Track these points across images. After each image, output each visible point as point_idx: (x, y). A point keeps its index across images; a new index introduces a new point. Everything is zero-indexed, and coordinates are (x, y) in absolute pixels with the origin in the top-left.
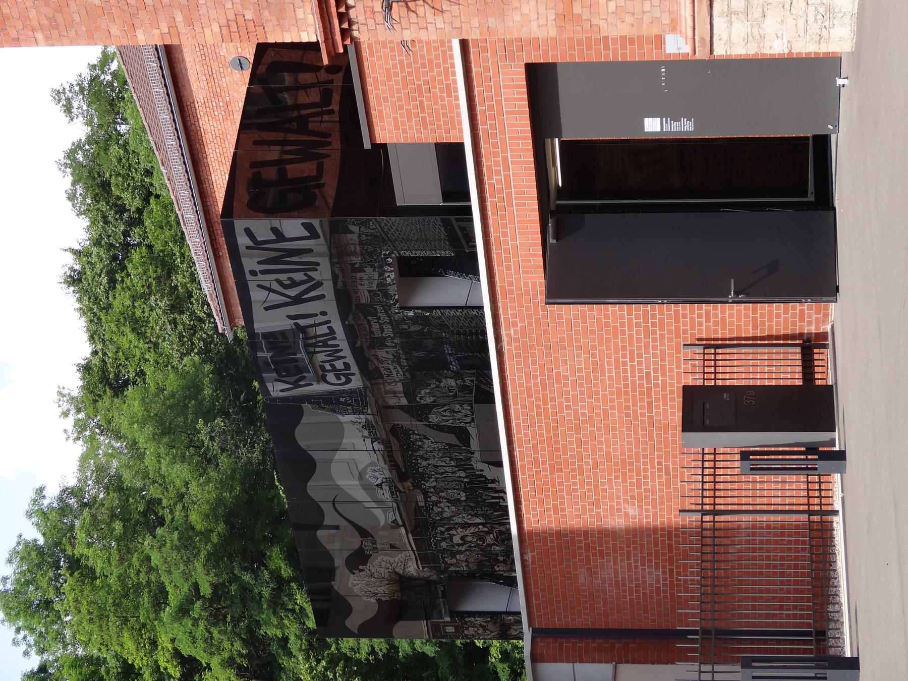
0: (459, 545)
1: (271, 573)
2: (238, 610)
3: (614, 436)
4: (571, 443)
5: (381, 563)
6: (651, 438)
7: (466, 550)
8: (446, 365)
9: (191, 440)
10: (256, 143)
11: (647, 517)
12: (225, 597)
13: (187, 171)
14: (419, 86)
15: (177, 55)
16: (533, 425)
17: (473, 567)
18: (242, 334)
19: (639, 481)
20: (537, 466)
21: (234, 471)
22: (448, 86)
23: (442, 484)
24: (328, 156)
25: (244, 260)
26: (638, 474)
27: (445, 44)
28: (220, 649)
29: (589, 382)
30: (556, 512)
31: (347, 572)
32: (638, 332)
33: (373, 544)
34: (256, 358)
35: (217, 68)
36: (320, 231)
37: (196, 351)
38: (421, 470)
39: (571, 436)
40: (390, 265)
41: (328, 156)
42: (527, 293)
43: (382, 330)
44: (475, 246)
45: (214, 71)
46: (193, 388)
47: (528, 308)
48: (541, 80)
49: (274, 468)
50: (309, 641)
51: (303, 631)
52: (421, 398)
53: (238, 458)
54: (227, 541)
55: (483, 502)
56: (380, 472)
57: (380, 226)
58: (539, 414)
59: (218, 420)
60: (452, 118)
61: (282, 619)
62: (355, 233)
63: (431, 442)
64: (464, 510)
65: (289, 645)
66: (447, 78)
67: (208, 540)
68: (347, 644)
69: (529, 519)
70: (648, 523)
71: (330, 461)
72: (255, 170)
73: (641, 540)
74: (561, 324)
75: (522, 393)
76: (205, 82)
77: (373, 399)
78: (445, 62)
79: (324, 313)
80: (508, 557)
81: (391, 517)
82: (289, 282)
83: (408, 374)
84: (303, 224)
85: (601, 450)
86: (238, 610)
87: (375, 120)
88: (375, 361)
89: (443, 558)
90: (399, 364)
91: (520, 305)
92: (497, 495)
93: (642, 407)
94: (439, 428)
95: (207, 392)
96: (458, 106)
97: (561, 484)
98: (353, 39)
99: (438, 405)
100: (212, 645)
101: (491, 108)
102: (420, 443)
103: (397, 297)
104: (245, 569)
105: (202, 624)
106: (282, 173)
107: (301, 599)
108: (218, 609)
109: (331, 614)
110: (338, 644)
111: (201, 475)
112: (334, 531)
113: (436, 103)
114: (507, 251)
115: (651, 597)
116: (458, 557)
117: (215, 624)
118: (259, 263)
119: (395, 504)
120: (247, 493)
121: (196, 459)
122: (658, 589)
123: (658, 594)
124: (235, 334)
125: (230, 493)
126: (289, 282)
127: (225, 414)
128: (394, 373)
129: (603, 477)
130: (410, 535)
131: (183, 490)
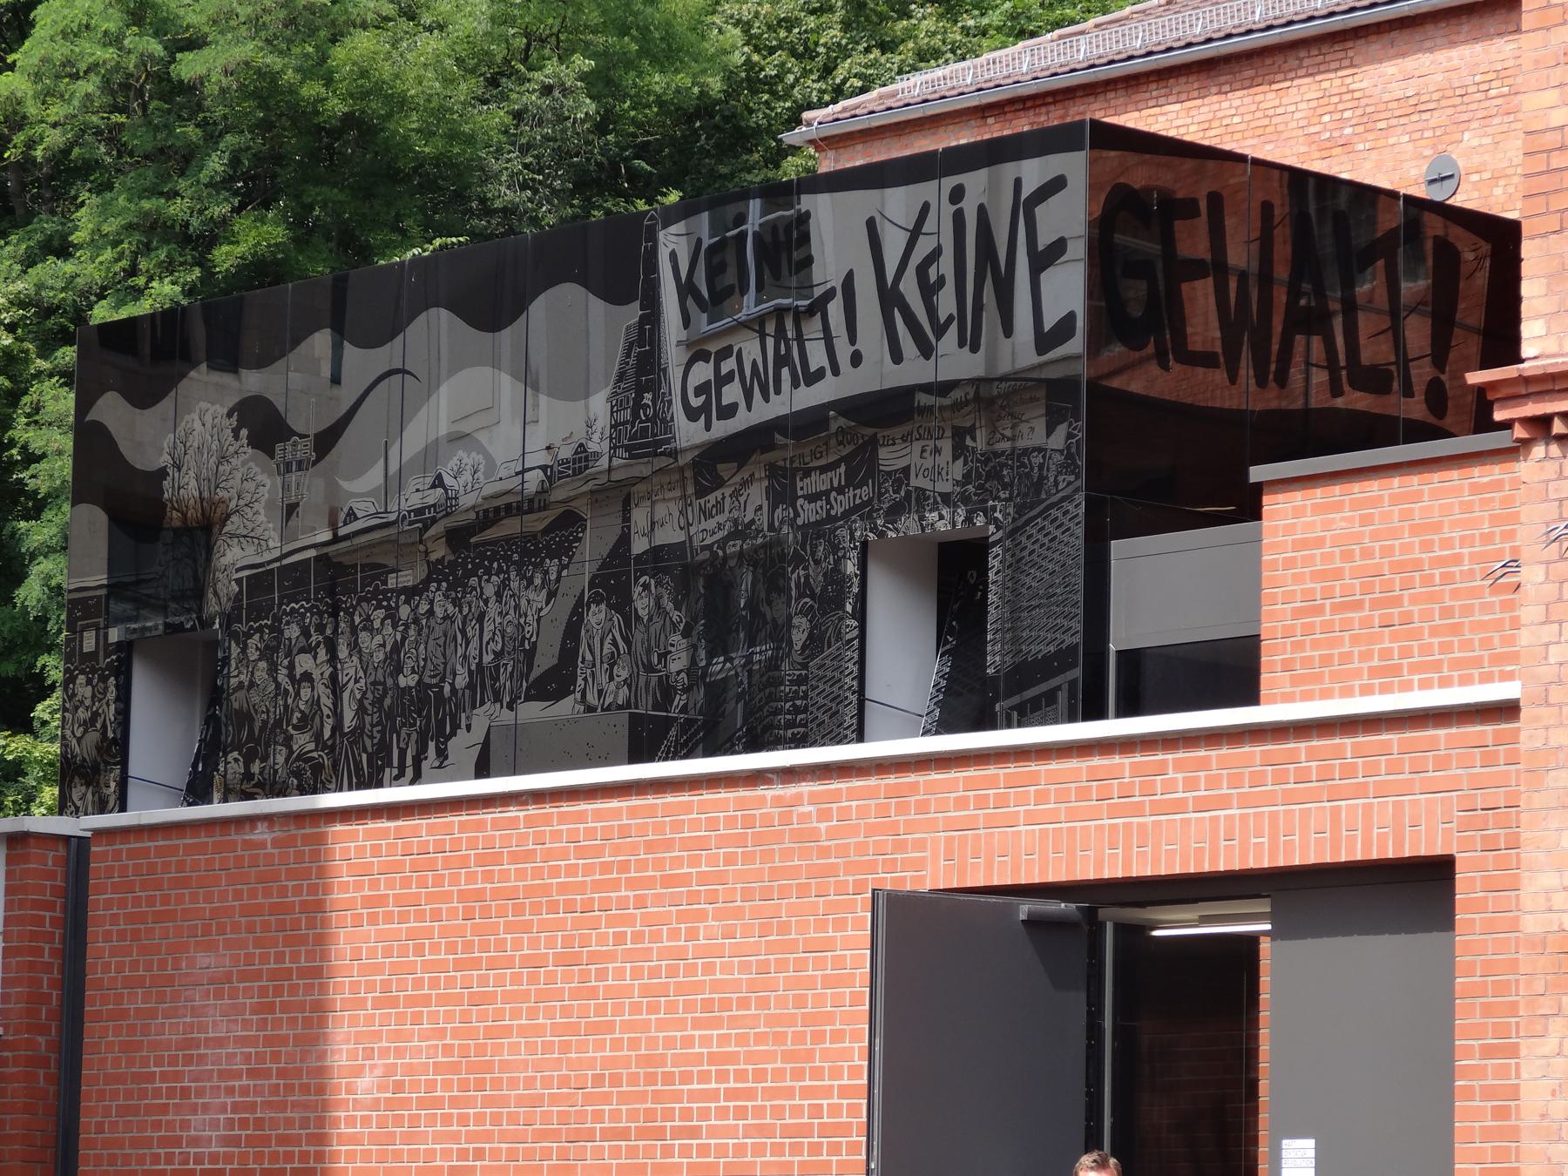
0: (291, 667)
1: (224, 222)
2: (139, 140)
3: (548, 1047)
4: (534, 943)
5: (253, 483)
6: (542, 1135)
7: (278, 685)
8: (719, 645)
9: (543, 41)
10: (1267, 207)
11: (351, 1121)
12: (169, 112)
13: (1189, 45)
14: (1397, 601)
15: (1465, 28)
16: (581, 852)
17: (237, 701)
18: (791, 168)
19: (437, 1103)
20: (482, 860)
21: (470, 140)
22: (1395, 670)
23: (438, 631)
24: (1233, 379)
25: (983, 174)
26: (454, 1102)
27: (1503, 663)
28: (45, 97)
29: (681, 989)
30: (369, 902)
31: (232, 401)
32: (797, 1111)
33: (300, 463)
34: (745, 195)
35: (1433, 123)
36: (1052, 355)
37: (756, 58)
38: (473, 581)
39: (551, 943)
40: (969, 520)
41: (1233, 379)
42: (900, 846)
43: (812, 498)
44: (1009, 726)
45: (1425, 116)
46: (667, 50)
47: (861, 848)
48: (1416, 889)
49: (473, 234)
50: (58, 307)
51: (84, 294)
52: (646, 587)
53: (499, 150)
54: (304, 118)
55: (394, 730)
56: (474, 480)
57: (1063, 499)
58: (606, 867)
59: (590, 106)
60: (1318, 678)
61: (115, 244)
62: (1045, 438)
63: (534, 608)
64: (374, 683)
65: (51, 259)
66: (1414, 669)
67: (306, 74)
68: (60, 401)
69: (353, 836)
70: (335, 1123)
71: (496, 364)
72: (1203, 205)
73: (295, 1105)
74: (821, 926)
75: (659, 828)
76: (1399, 94)
77: (645, 471)
78: (1456, 664)
79: (856, 359)
80: (259, 785)
81: (362, 507)
82: (933, 278)
83: (706, 554)
84: (1071, 316)
85: (516, 1014)
86: (139, 140)
87: (1318, 494)
88: (737, 479)
89: (260, 630)
90: (733, 535)
91: (871, 830)
92: (409, 761)
93: (615, 1115)
94: (573, 630)
95: (657, 81)
96: (1347, 693)
97: (436, 916)
98: (1526, 444)
99: (628, 626)
100: (58, 77)
101: (1348, 771)
102: (538, 581)
103: (891, 534)
104: (235, 161)
105: (110, 54)
106: (1196, 269)
107: (165, 291)
108: (140, 93)
109: (139, 359)
110: (51, 376)
111: (459, 61)
112: (326, 371)
113: (1355, 640)
114: (1001, 802)
115: (157, 1125)
116: (263, 664)
117: (106, 84)
118: (982, 210)
119: (393, 517)
120: (415, 169)
121: (499, 51)
122: (177, 1142)
123: (163, 1142)
124: (794, 150)
125: (418, 131)
126: (933, 278)
127: (601, 127)
128: (711, 524)
129: (449, 1017)
130: (312, 553)
131: (427, 19)
